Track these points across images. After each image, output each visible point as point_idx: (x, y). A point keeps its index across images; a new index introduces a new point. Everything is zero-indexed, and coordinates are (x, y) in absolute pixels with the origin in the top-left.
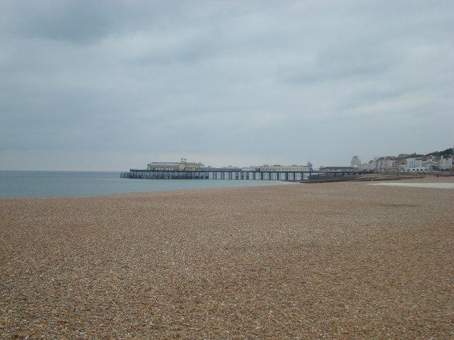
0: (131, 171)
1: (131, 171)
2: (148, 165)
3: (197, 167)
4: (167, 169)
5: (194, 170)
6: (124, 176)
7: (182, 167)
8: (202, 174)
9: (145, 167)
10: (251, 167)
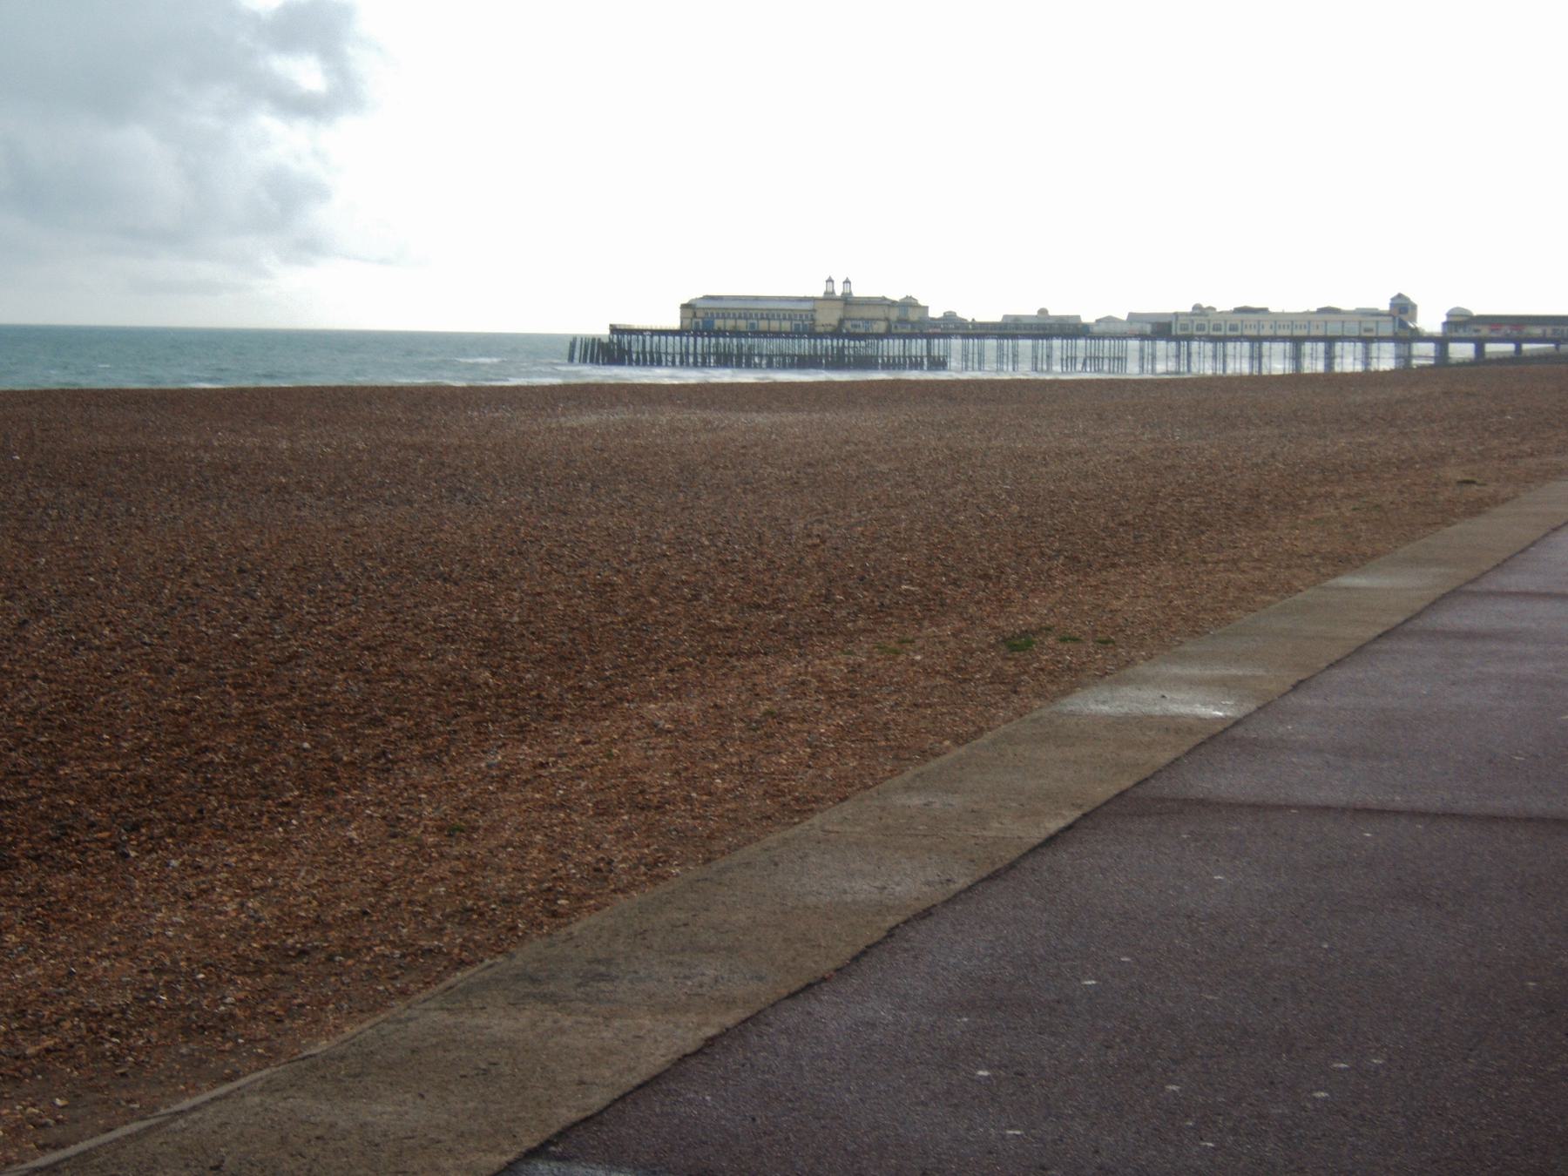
0: (614, 330)
1: (614, 330)
2: (684, 307)
3: (894, 314)
4: (763, 325)
5: (880, 327)
9: (674, 322)
10: (1133, 317)
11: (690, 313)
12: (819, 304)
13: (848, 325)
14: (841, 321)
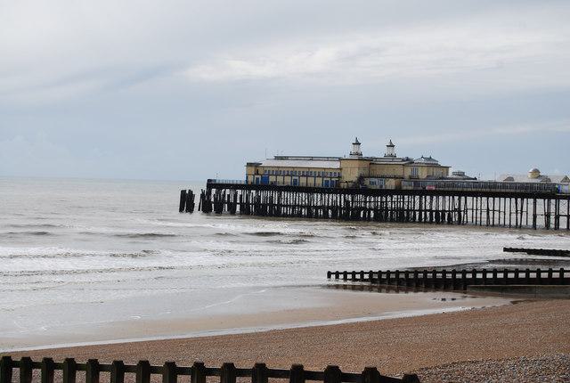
1: (211, 184)
2: (249, 165)
6: (216, 200)
7: (351, 175)
8: (445, 203)
9: (239, 175)
11: (253, 170)
12: (344, 164)
13: (367, 182)
14: (361, 178)
